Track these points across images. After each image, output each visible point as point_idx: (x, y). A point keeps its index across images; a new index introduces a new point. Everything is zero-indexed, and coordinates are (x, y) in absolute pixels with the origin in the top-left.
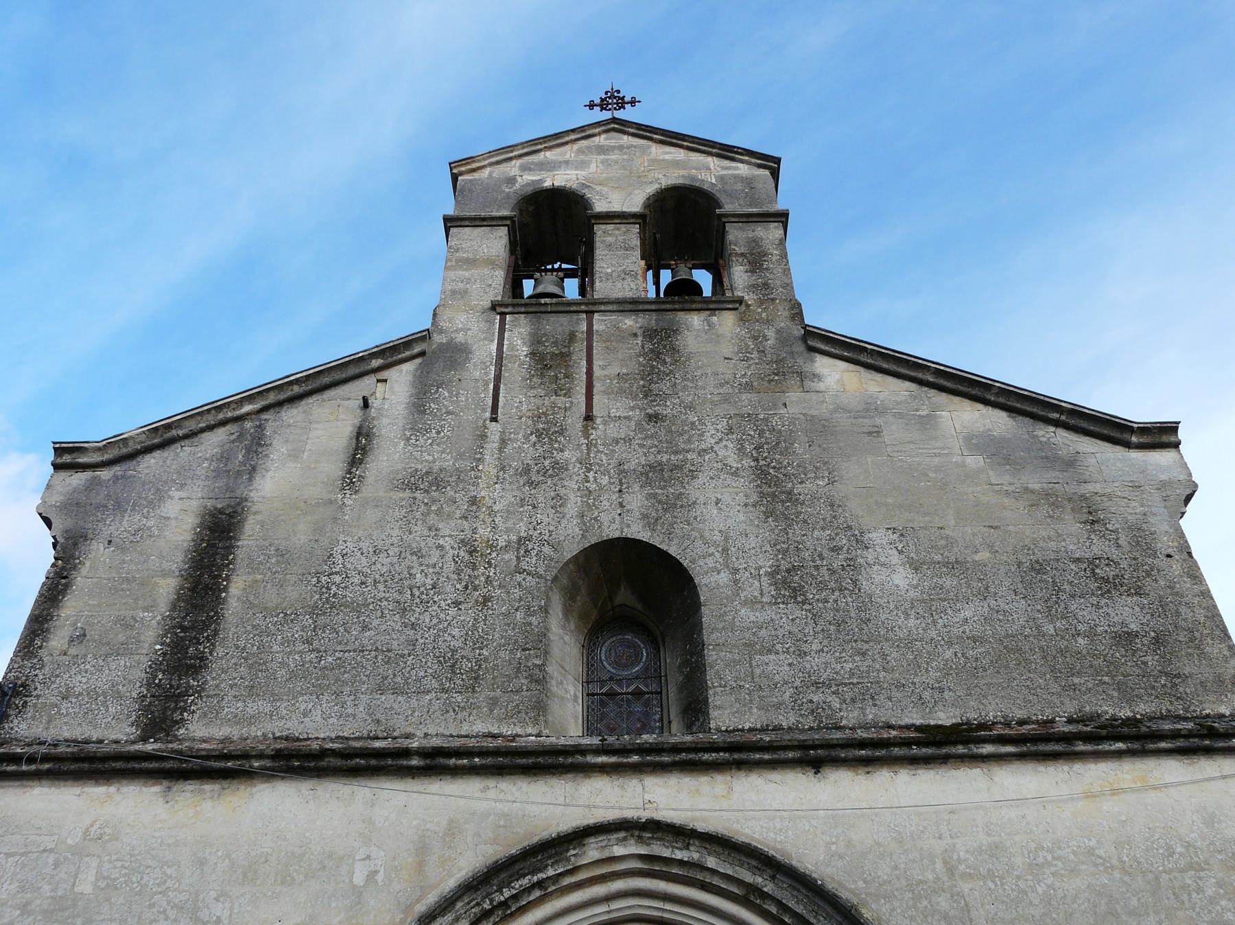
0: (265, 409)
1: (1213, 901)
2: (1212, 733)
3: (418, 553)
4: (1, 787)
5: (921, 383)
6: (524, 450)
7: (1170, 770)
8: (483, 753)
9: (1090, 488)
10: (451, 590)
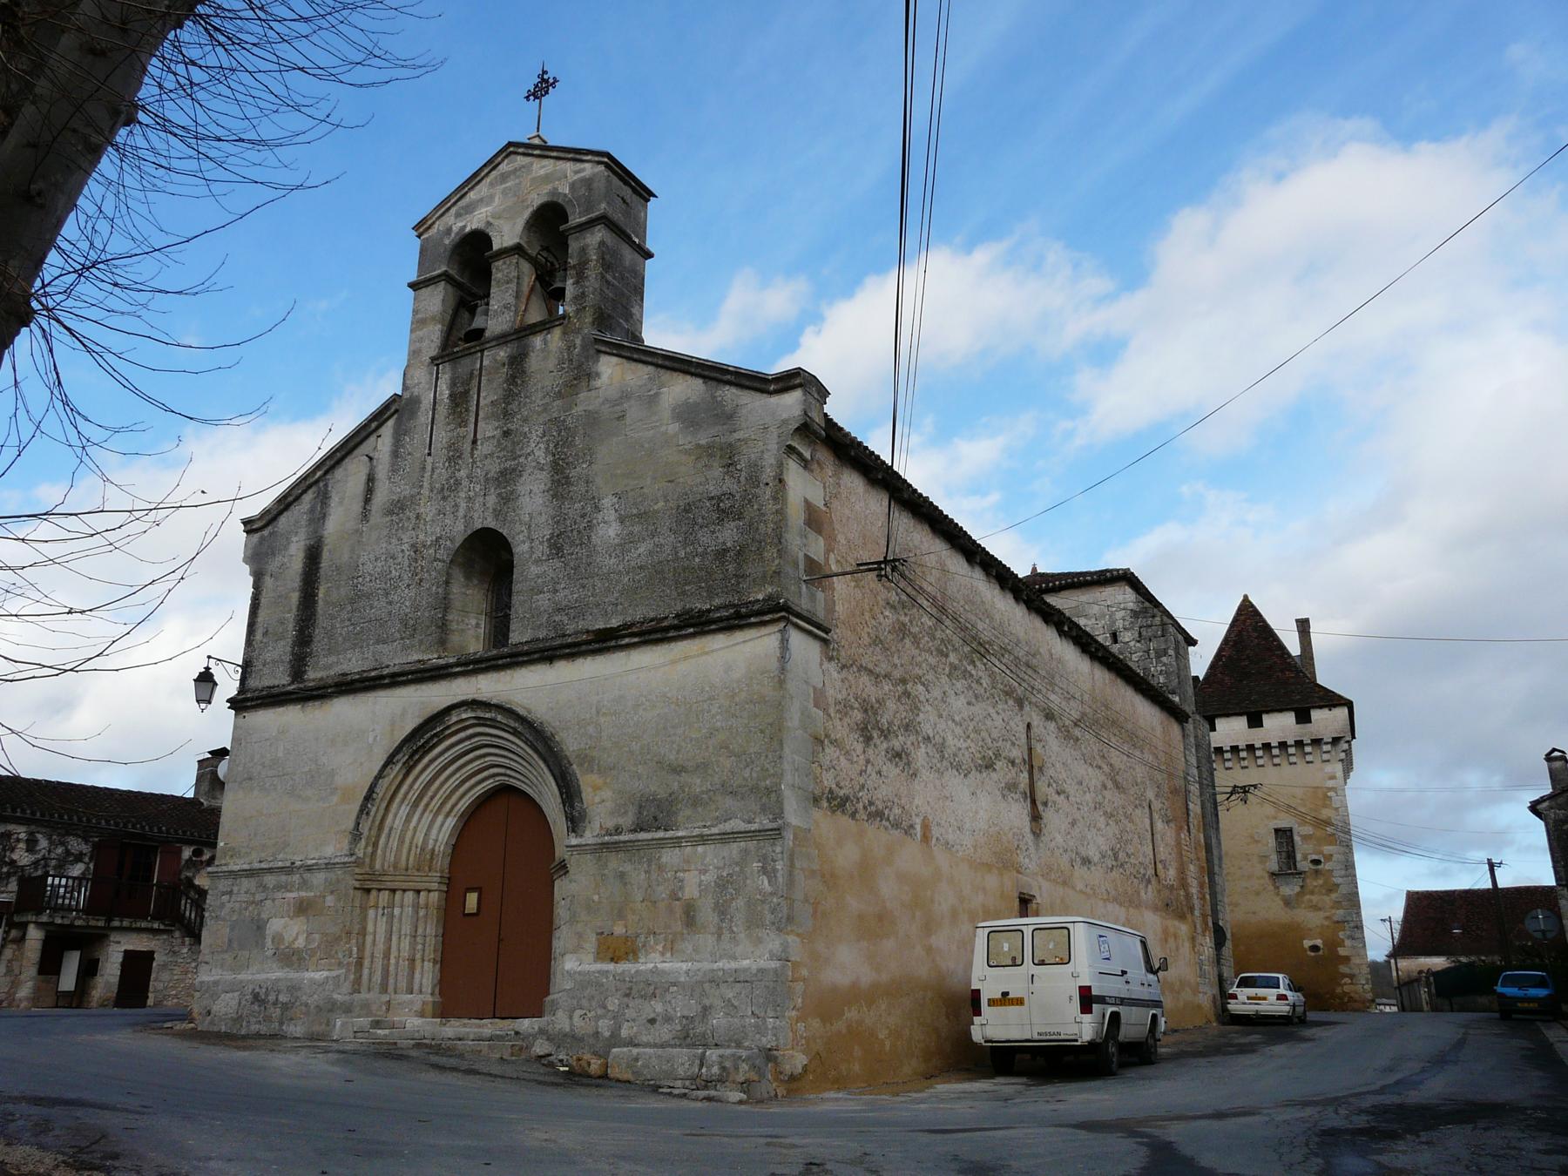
0: (326, 473)
1: (713, 716)
2: (738, 616)
3: (393, 558)
5: (657, 366)
6: (442, 473)
7: (719, 641)
8: (412, 673)
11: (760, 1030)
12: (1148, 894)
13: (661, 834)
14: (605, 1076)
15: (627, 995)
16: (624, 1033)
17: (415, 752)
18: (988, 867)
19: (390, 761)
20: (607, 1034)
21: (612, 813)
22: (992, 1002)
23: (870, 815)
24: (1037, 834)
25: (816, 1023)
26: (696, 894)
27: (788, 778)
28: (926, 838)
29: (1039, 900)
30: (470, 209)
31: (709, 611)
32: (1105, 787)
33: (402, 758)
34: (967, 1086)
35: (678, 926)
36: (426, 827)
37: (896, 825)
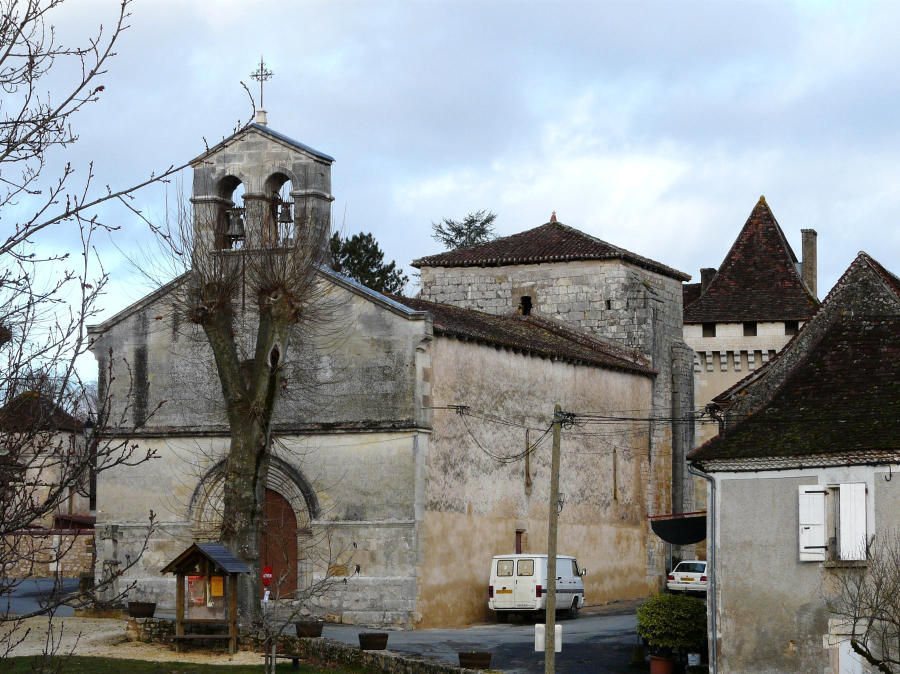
4: (837, 671)
7: (384, 437)
9: (392, 338)
10: (207, 378)
11: (405, 604)
12: (607, 514)
13: (359, 522)
14: (341, 622)
16: (344, 605)
18: (500, 519)
22: (498, 592)
23: (447, 508)
24: (528, 494)
25: (425, 601)
26: (376, 548)
27: (416, 501)
28: (470, 512)
29: (528, 531)
30: (226, 159)
31: (380, 422)
32: (578, 450)
34: (486, 627)
35: (368, 562)
37: (457, 510)
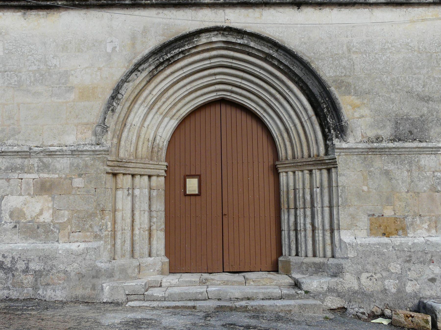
13: (416, 144)
15: (409, 261)
17: (161, 64)
19: (136, 68)
20: (394, 290)
21: (371, 126)
33: (148, 68)
36: (153, 124)
